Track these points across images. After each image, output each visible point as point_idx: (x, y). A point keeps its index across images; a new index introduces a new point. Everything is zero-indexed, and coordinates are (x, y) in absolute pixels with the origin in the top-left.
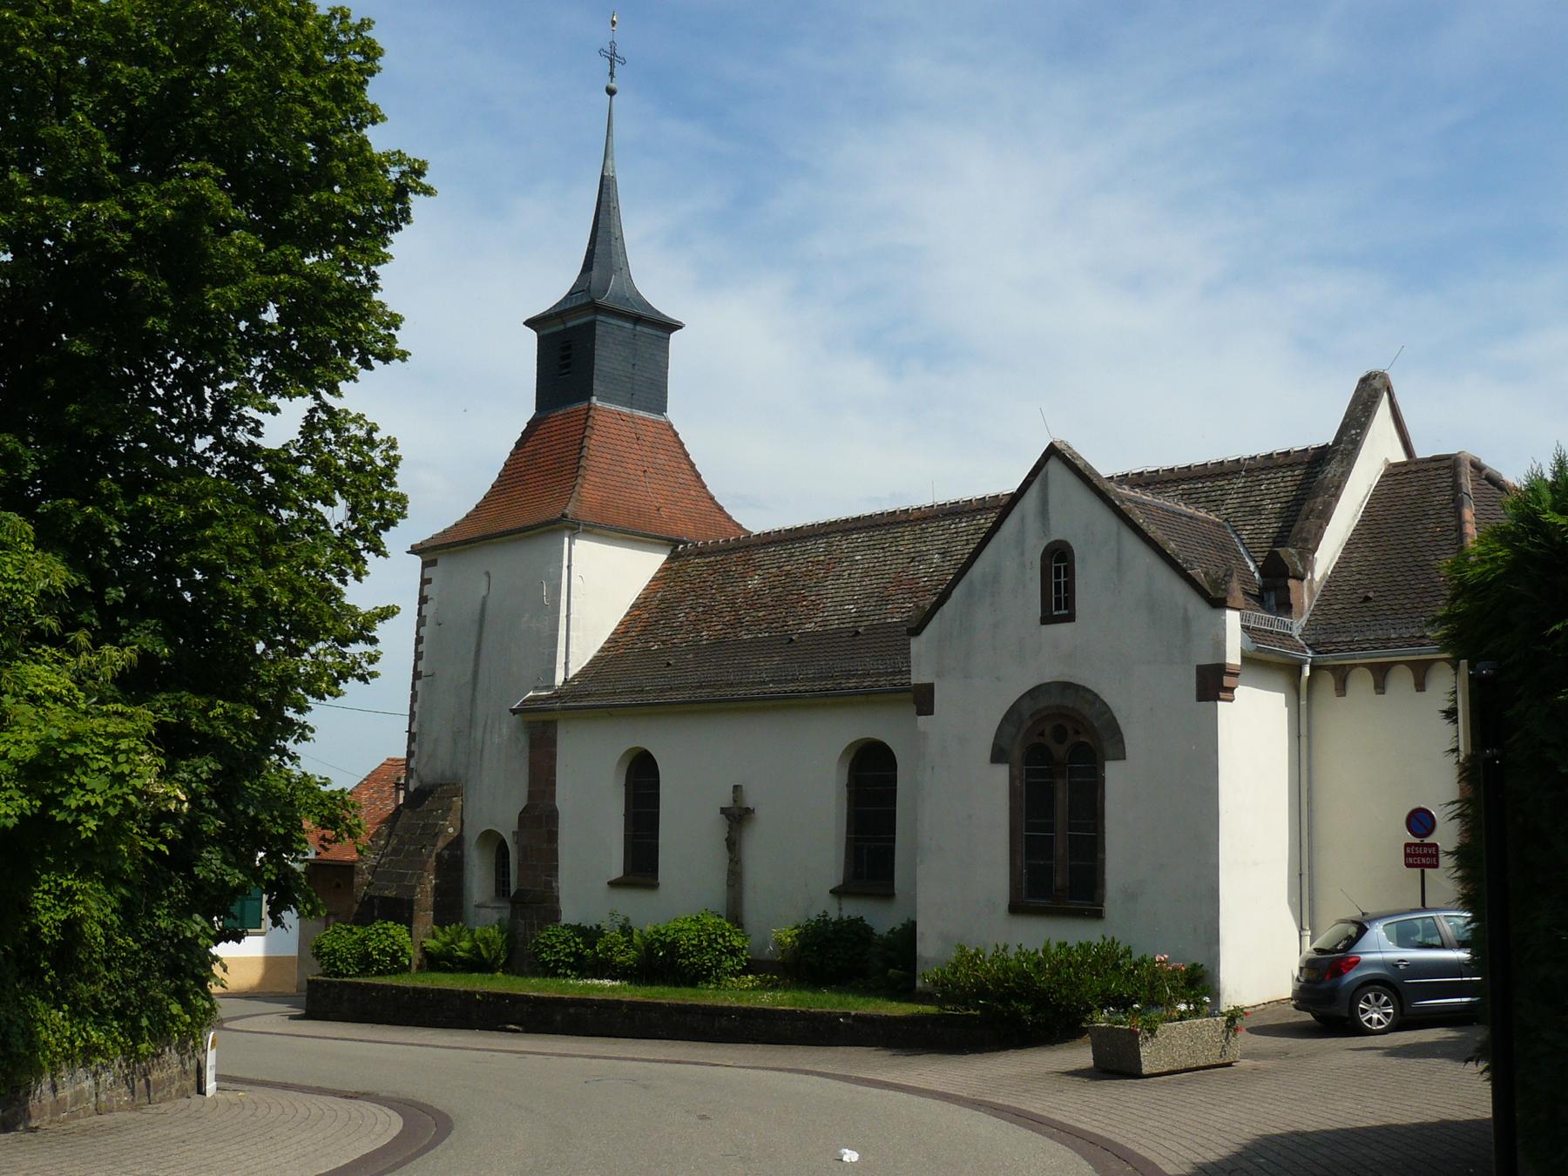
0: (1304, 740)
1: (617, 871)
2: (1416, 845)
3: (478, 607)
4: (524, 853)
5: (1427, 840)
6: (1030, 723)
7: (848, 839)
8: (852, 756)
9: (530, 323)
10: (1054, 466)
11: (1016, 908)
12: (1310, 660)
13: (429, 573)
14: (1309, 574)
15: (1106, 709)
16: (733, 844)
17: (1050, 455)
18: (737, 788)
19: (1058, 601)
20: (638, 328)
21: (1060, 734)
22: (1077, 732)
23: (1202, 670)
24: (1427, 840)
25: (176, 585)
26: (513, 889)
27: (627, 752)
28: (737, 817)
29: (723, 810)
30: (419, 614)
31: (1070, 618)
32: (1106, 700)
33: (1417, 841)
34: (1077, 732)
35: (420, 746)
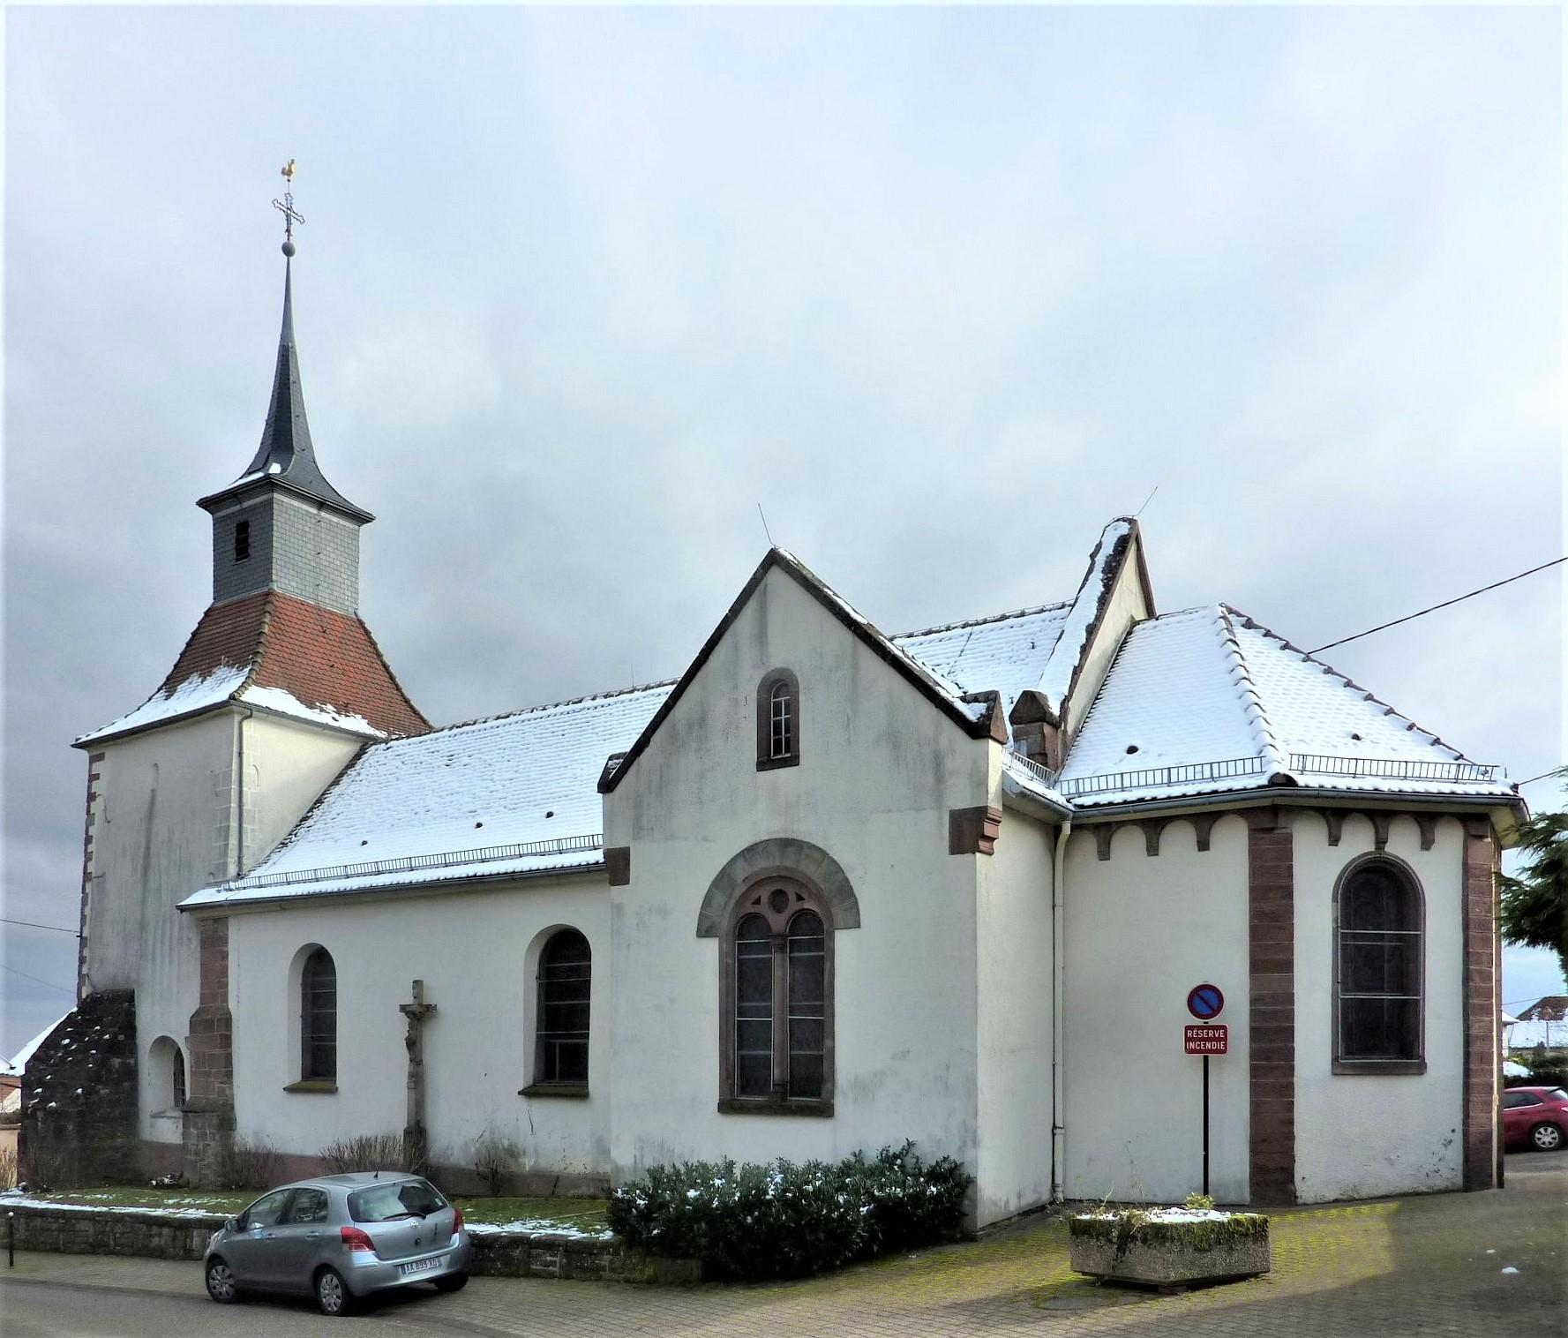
0: (1059, 910)
1: (296, 1077)
2: (1199, 1027)
3: (147, 799)
4: (198, 1060)
5: (1212, 1022)
6: (743, 888)
7: (539, 1037)
8: (543, 943)
9: (206, 503)
10: (776, 575)
11: (728, 1106)
12: (1071, 815)
13: (97, 768)
14: (1063, 725)
15: (836, 868)
16: (413, 1044)
17: (771, 565)
18: (418, 984)
19: (778, 743)
20: (323, 514)
21: (778, 900)
22: (800, 898)
23: (958, 818)
24: (1212, 1022)
25: (1512, 1274)
26: (188, 1096)
27: (300, 950)
28: (419, 1015)
29: (403, 1008)
30: (88, 812)
31: (793, 761)
32: (835, 858)
33: (1200, 1022)
34: (800, 898)
35: (91, 951)
